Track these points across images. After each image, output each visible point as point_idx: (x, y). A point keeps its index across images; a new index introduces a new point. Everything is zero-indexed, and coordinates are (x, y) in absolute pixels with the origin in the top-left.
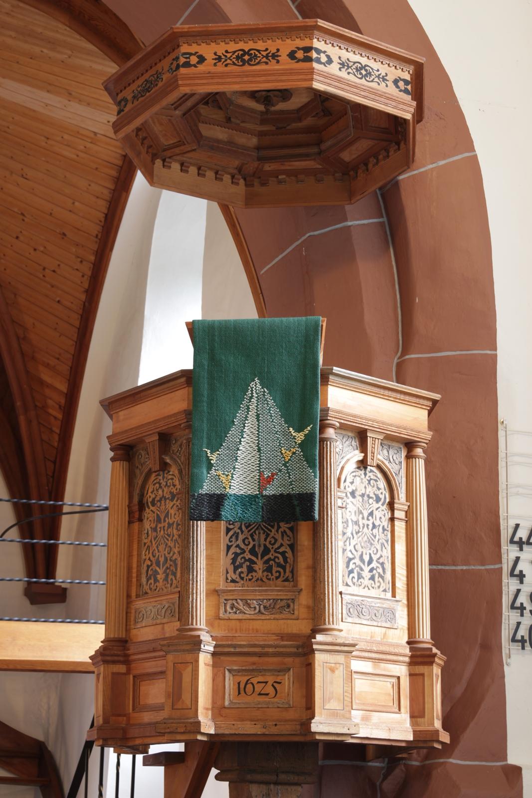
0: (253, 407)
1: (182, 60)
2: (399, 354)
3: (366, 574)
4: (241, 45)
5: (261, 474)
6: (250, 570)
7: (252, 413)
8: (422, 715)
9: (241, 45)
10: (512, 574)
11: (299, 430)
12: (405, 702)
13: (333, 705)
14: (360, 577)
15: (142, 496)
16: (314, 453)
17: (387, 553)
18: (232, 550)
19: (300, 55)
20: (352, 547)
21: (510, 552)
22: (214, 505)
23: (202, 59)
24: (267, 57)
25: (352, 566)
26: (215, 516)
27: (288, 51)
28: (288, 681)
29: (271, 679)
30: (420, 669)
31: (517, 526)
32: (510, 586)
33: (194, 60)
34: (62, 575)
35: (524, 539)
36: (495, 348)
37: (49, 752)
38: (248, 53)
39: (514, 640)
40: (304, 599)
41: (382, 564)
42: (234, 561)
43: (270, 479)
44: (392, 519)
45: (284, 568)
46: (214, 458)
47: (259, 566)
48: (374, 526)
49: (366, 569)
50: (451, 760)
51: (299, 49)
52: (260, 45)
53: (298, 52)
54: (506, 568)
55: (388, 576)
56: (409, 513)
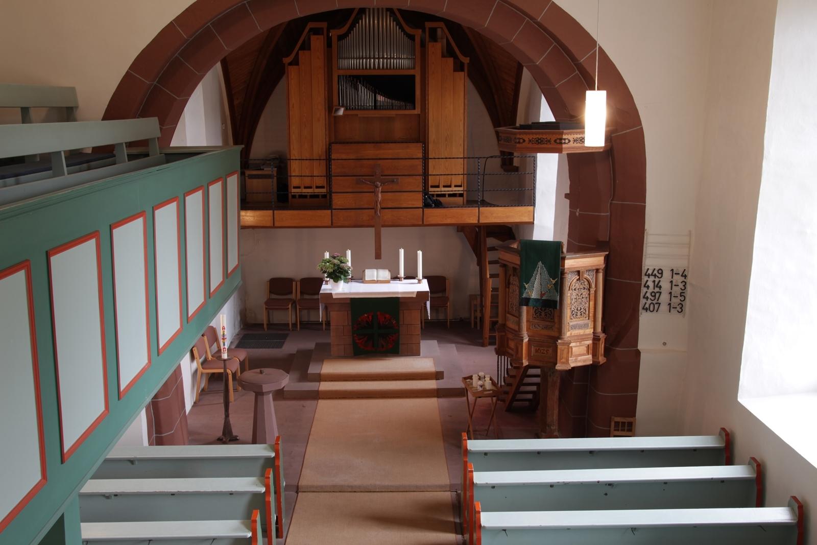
0: (539, 270)
1: (518, 141)
2: (611, 199)
3: (579, 314)
4: (537, 136)
5: (541, 292)
6: (540, 315)
7: (539, 272)
8: (596, 356)
9: (537, 136)
10: (645, 286)
11: (553, 279)
12: (590, 351)
13: (563, 360)
14: (576, 315)
15: (509, 280)
16: (559, 287)
17: (587, 305)
18: (535, 308)
19: (558, 141)
20: (574, 307)
21: (645, 278)
22: (526, 301)
23: (524, 141)
24: (547, 141)
25: (574, 312)
26: (527, 305)
27: (554, 140)
28: (551, 350)
29: (546, 349)
30: (596, 342)
31: (648, 269)
32: (644, 290)
33: (521, 141)
34: (516, 162)
35: (650, 274)
36: (645, 203)
37: (513, 233)
38: (540, 139)
39: (643, 309)
40: (556, 326)
41: (585, 310)
42: (535, 311)
43: (544, 294)
44: (589, 294)
45: (551, 315)
46: (527, 286)
47: (543, 314)
48: (582, 298)
49: (579, 312)
50: (617, 349)
51: (558, 139)
52: (544, 137)
53: (468, 460)
54: (643, 283)
55: (587, 312)
56: (596, 292)
